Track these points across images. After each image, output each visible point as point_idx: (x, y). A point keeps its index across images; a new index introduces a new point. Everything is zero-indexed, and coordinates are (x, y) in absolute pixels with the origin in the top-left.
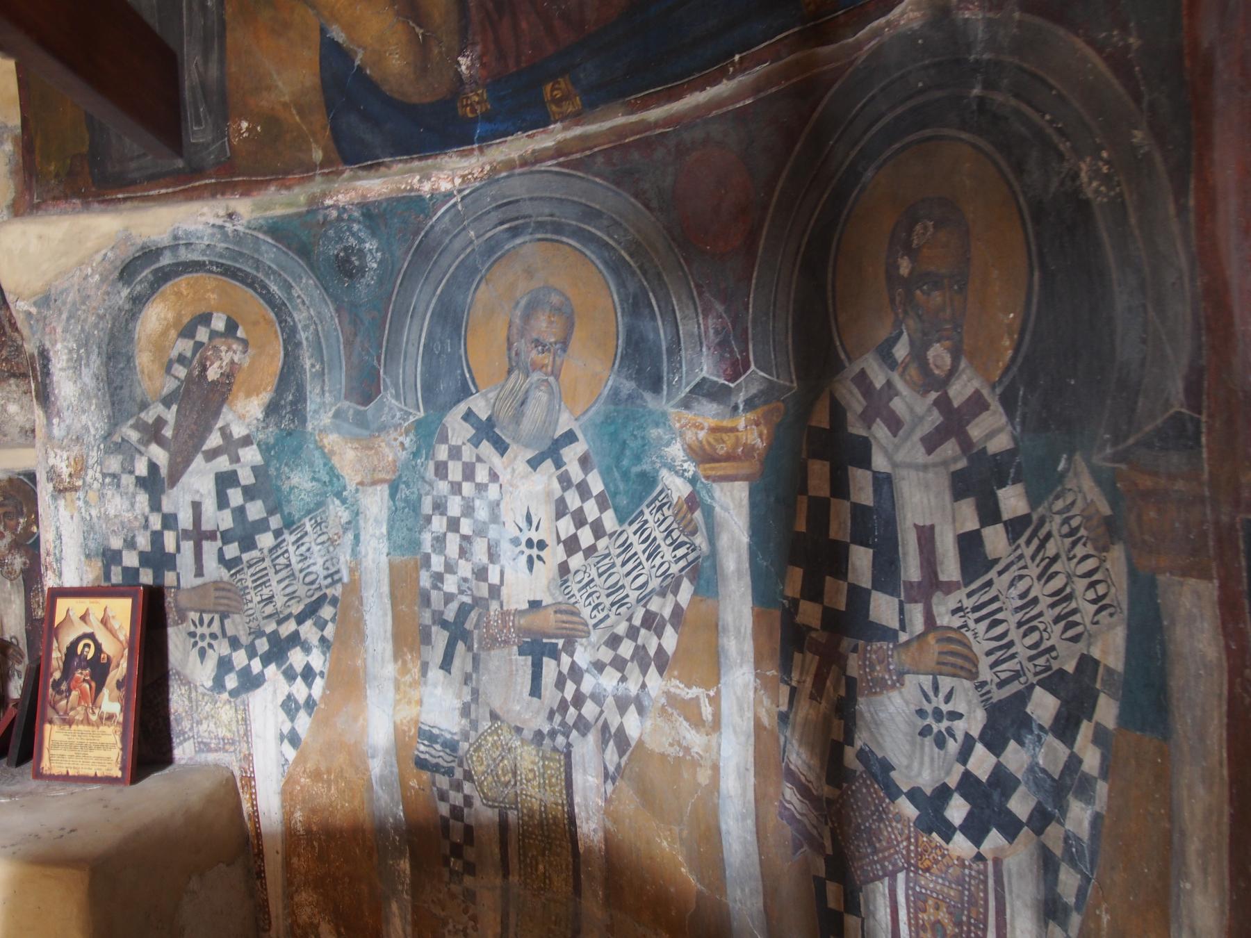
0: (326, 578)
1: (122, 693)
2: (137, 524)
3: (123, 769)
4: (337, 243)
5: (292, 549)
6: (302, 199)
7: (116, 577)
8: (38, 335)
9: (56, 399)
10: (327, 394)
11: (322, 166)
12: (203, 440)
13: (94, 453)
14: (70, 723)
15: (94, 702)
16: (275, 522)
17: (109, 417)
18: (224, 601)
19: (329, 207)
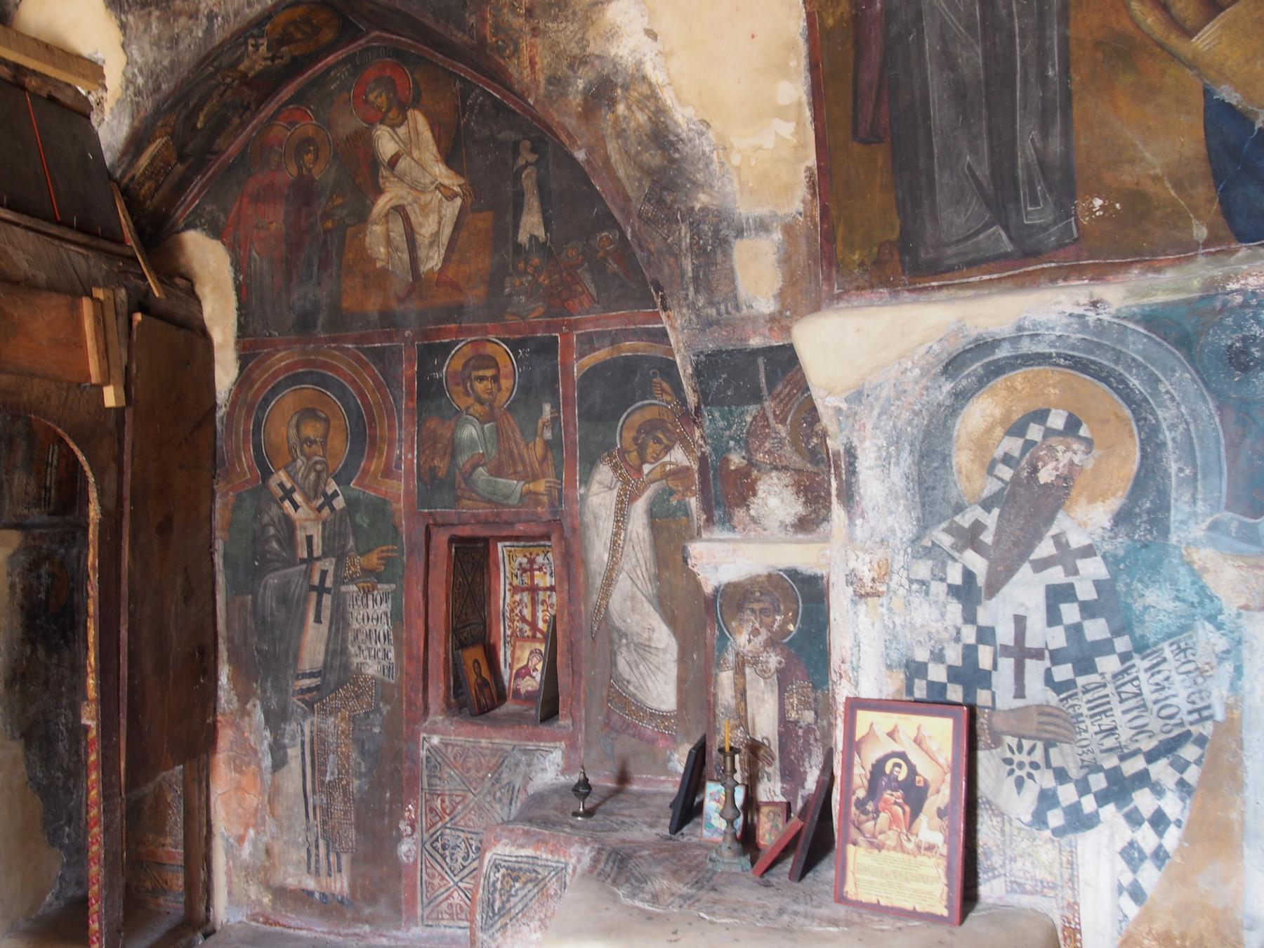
0: (1190, 713)
1: (945, 823)
2: (947, 636)
3: (949, 907)
4: (1234, 332)
5: (1143, 676)
6: (1196, 283)
7: (920, 691)
8: (846, 432)
9: (861, 498)
10: (1200, 503)
11: (1206, 244)
12: (1031, 547)
13: (901, 558)
14: (880, 847)
15: (909, 828)
16: (1122, 644)
17: (918, 519)
18: (1051, 728)
19: (1232, 292)
